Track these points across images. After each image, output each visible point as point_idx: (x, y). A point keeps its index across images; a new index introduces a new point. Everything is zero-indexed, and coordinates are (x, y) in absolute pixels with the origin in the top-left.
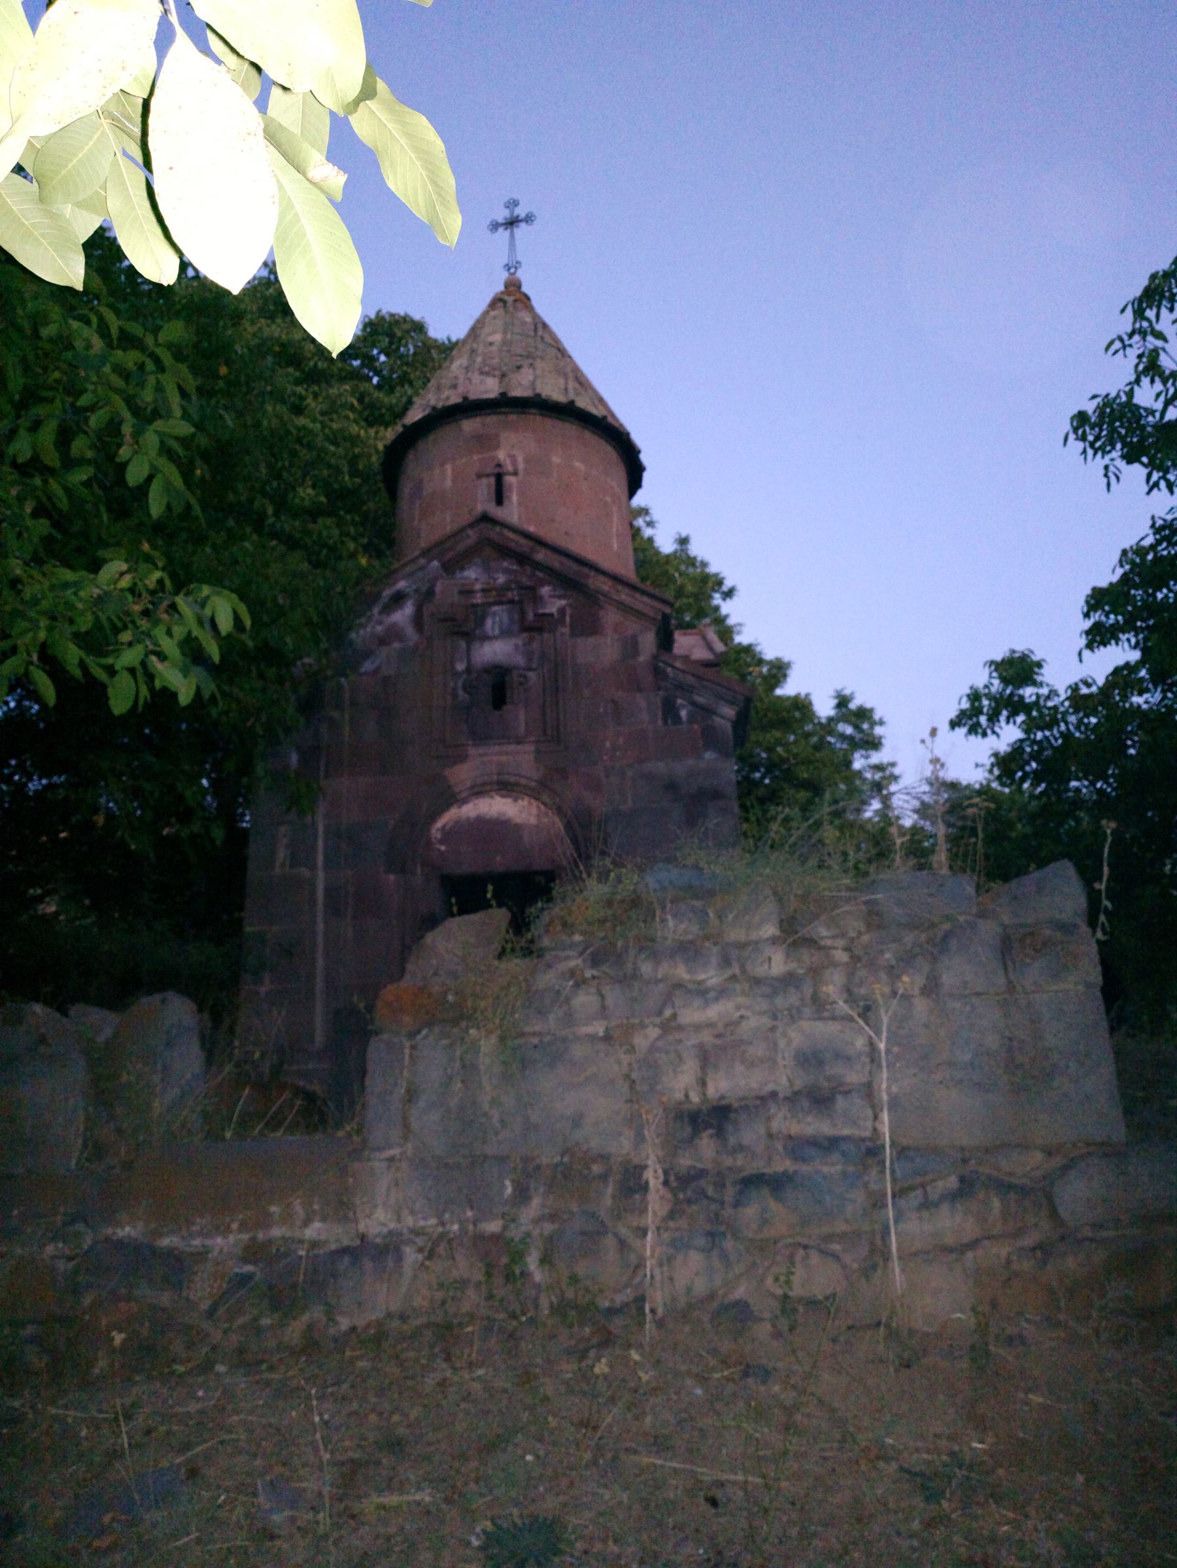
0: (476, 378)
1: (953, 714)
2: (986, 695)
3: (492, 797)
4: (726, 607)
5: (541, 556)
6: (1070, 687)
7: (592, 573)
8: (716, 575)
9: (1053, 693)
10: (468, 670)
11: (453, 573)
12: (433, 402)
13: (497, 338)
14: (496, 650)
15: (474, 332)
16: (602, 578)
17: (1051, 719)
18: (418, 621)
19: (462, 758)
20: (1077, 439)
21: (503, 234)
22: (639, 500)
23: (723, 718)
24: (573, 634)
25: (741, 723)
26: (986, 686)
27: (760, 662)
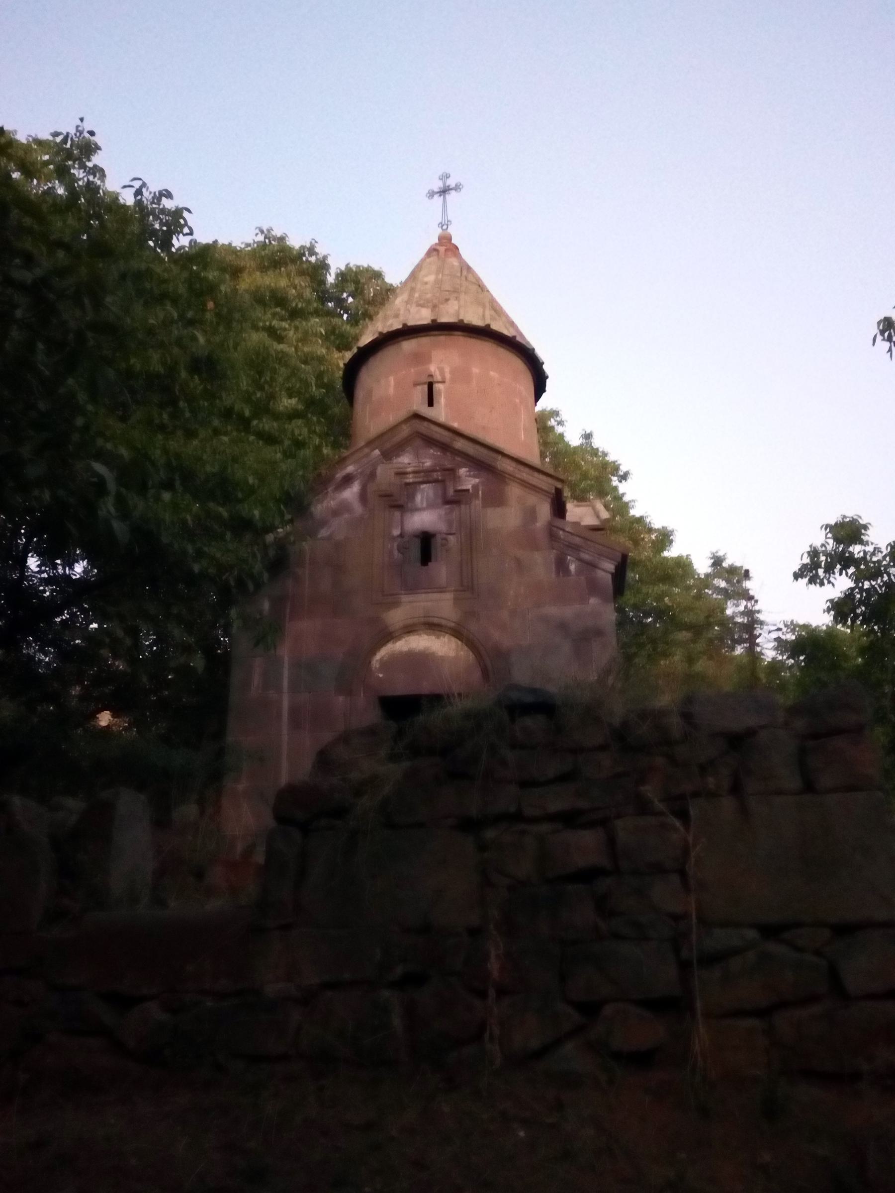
0: (413, 309)
1: (796, 568)
2: (823, 552)
4: (622, 488)
5: (460, 444)
6: (890, 544)
7: (500, 457)
8: (614, 462)
9: (877, 550)
10: (401, 536)
11: (391, 459)
12: (380, 329)
13: (431, 278)
14: (425, 517)
15: (413, 276)
16: (508, 461)
17: (875, 572)
18: (363, 496)
19: (396, 604)
20: (884, 340)
21: (438, 200)
22: (545, 403)
23: (604, 570)
24: (485, 506)
25: (619, 575)
26: (823, 545)
27: (650, 530)
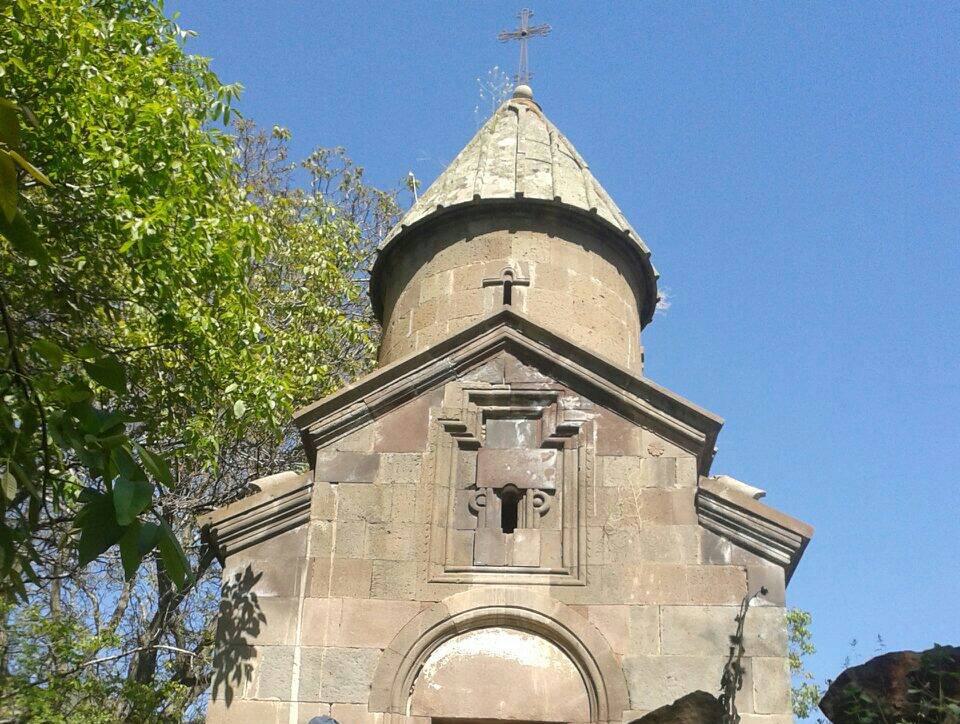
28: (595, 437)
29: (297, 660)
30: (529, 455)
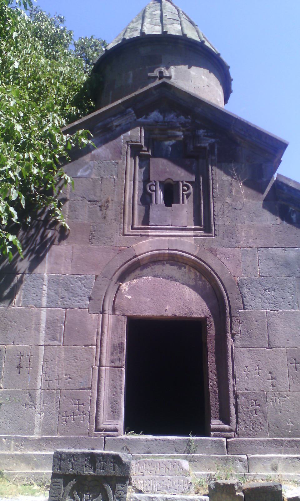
3: (164, 264)
28: (216, 152)
29: (46, 283)
30: (65, 140)
